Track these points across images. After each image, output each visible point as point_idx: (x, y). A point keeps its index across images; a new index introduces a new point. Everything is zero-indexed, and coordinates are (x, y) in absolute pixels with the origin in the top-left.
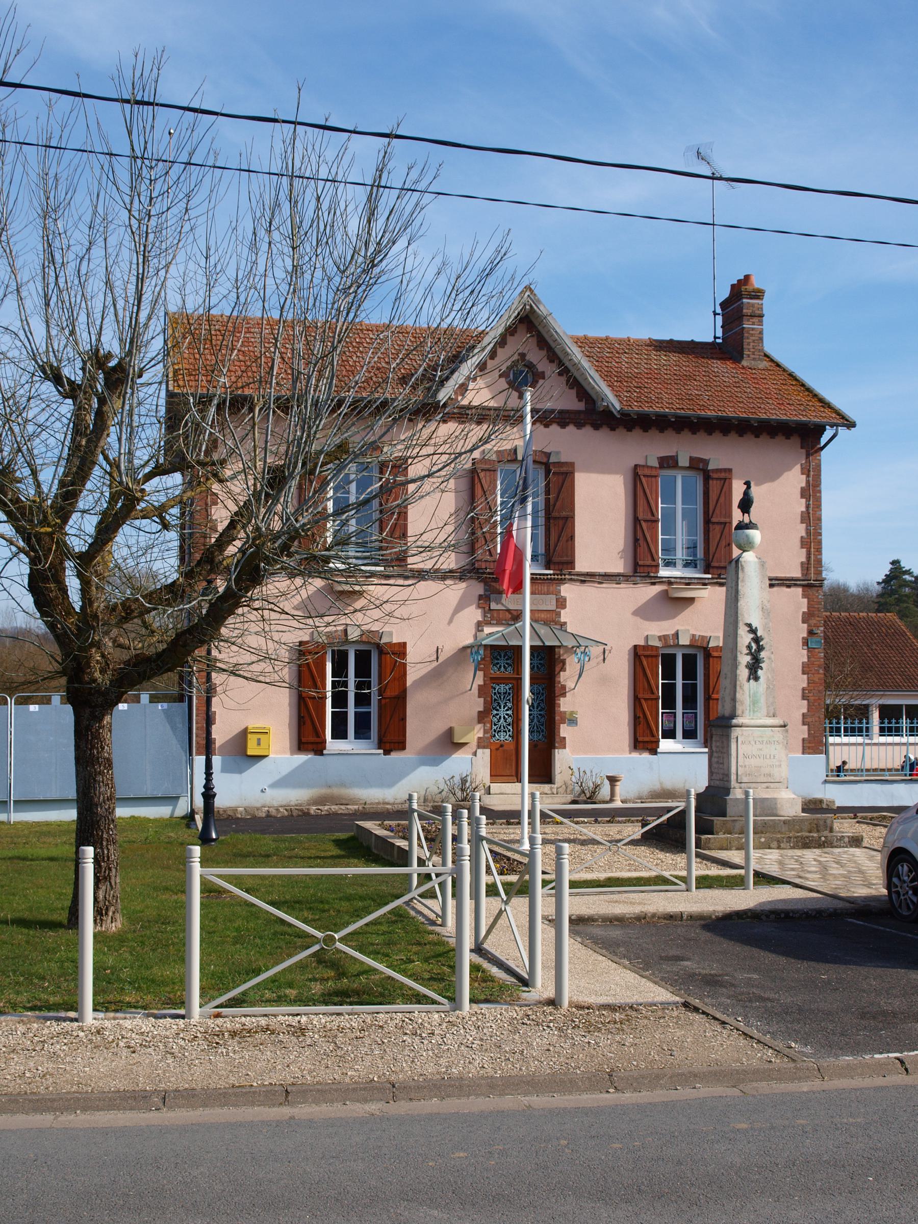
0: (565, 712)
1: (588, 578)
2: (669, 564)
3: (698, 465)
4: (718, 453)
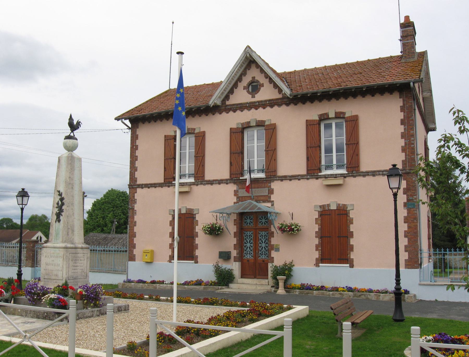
0: (273, 245)
1: (284, 178)
2: (329, 167)
3: (339, 116)
4: (350, 108)
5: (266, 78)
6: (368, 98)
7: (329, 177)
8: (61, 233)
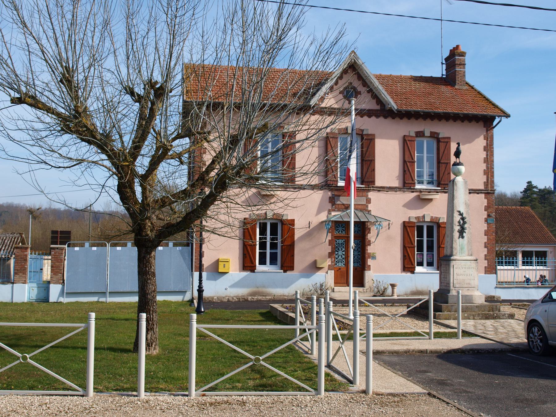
1: (381, 189)
2: (421, 182)
3: (434, 135)
4: (444, 130)
6: (458, 124)
7: (424, 192)
8: (466, 248)
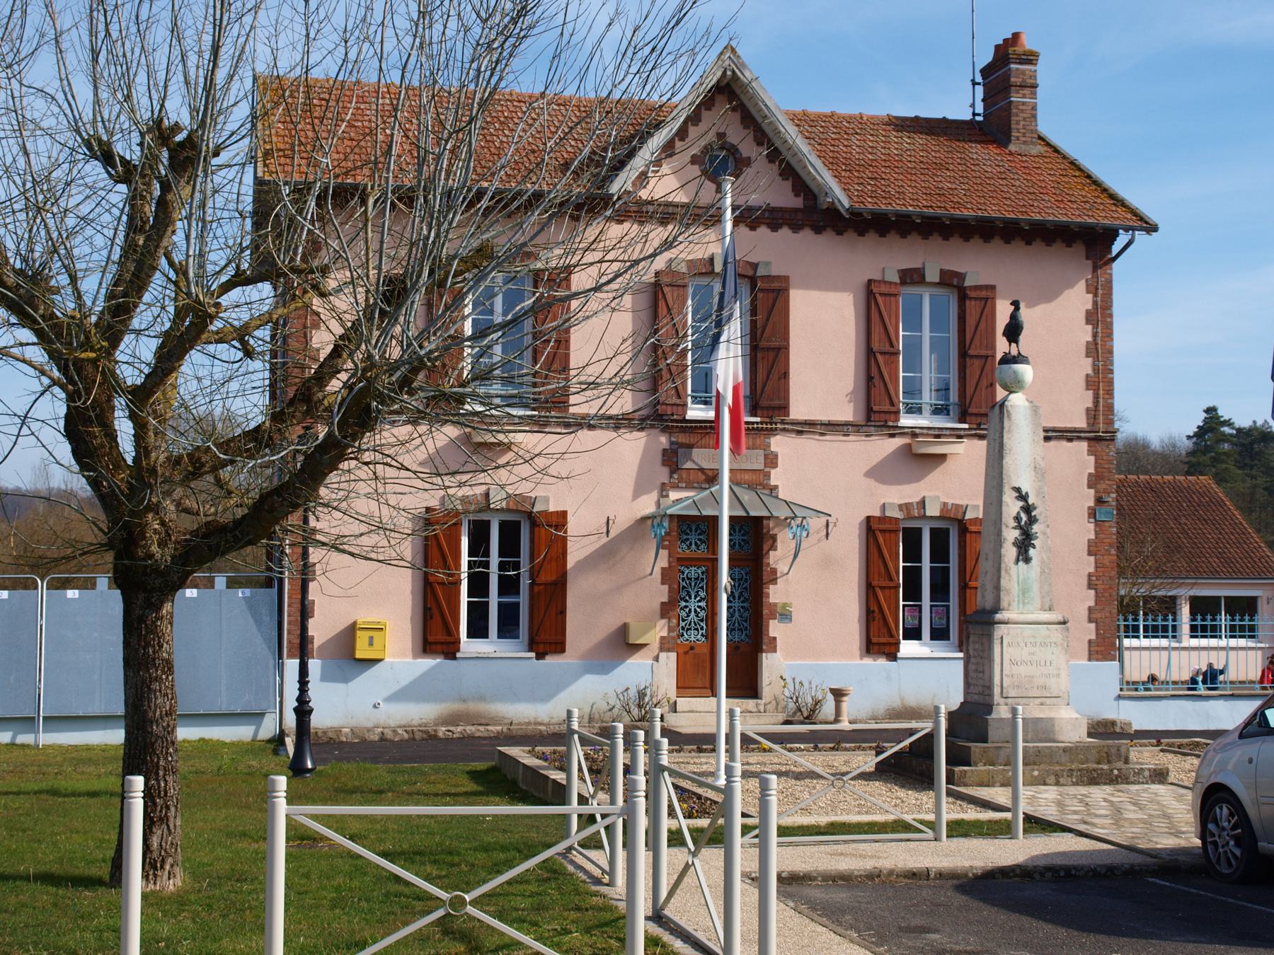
0: (775, 605)
2: (914, 410)
3: (951, 280)
4: (977, 265)
5: (760, 144)
8: (1035, 588)
